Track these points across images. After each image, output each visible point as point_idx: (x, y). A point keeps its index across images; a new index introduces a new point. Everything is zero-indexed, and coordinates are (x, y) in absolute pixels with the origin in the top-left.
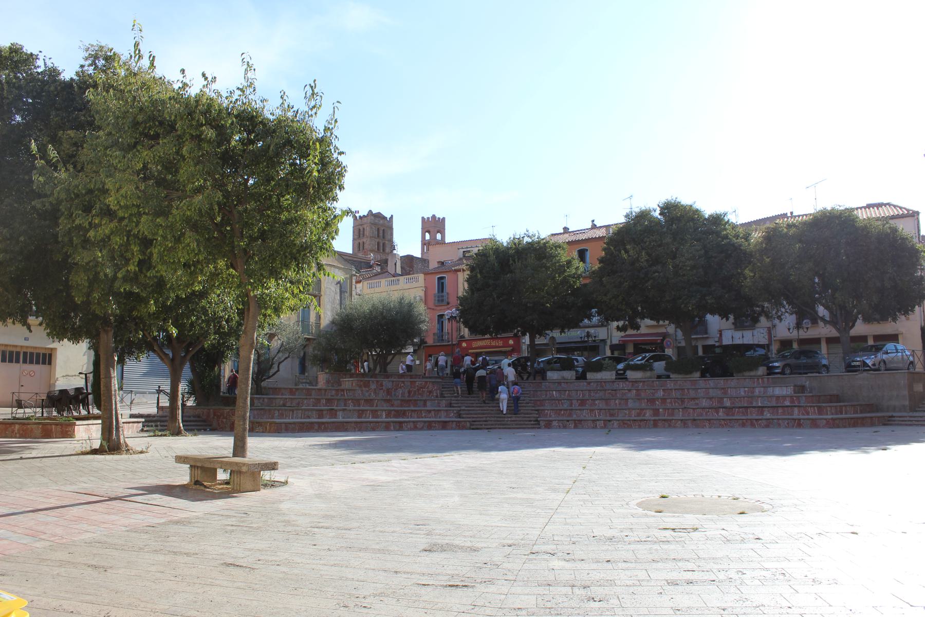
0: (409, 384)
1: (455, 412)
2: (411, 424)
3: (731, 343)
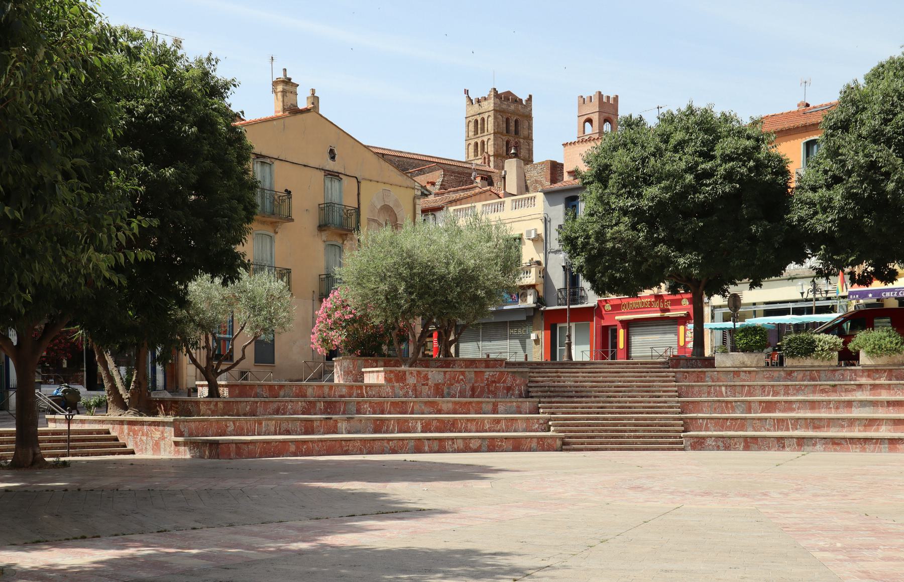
0: (473, 375)
1: (541, 421)
2: (460, 441)
3: (581, 360)
